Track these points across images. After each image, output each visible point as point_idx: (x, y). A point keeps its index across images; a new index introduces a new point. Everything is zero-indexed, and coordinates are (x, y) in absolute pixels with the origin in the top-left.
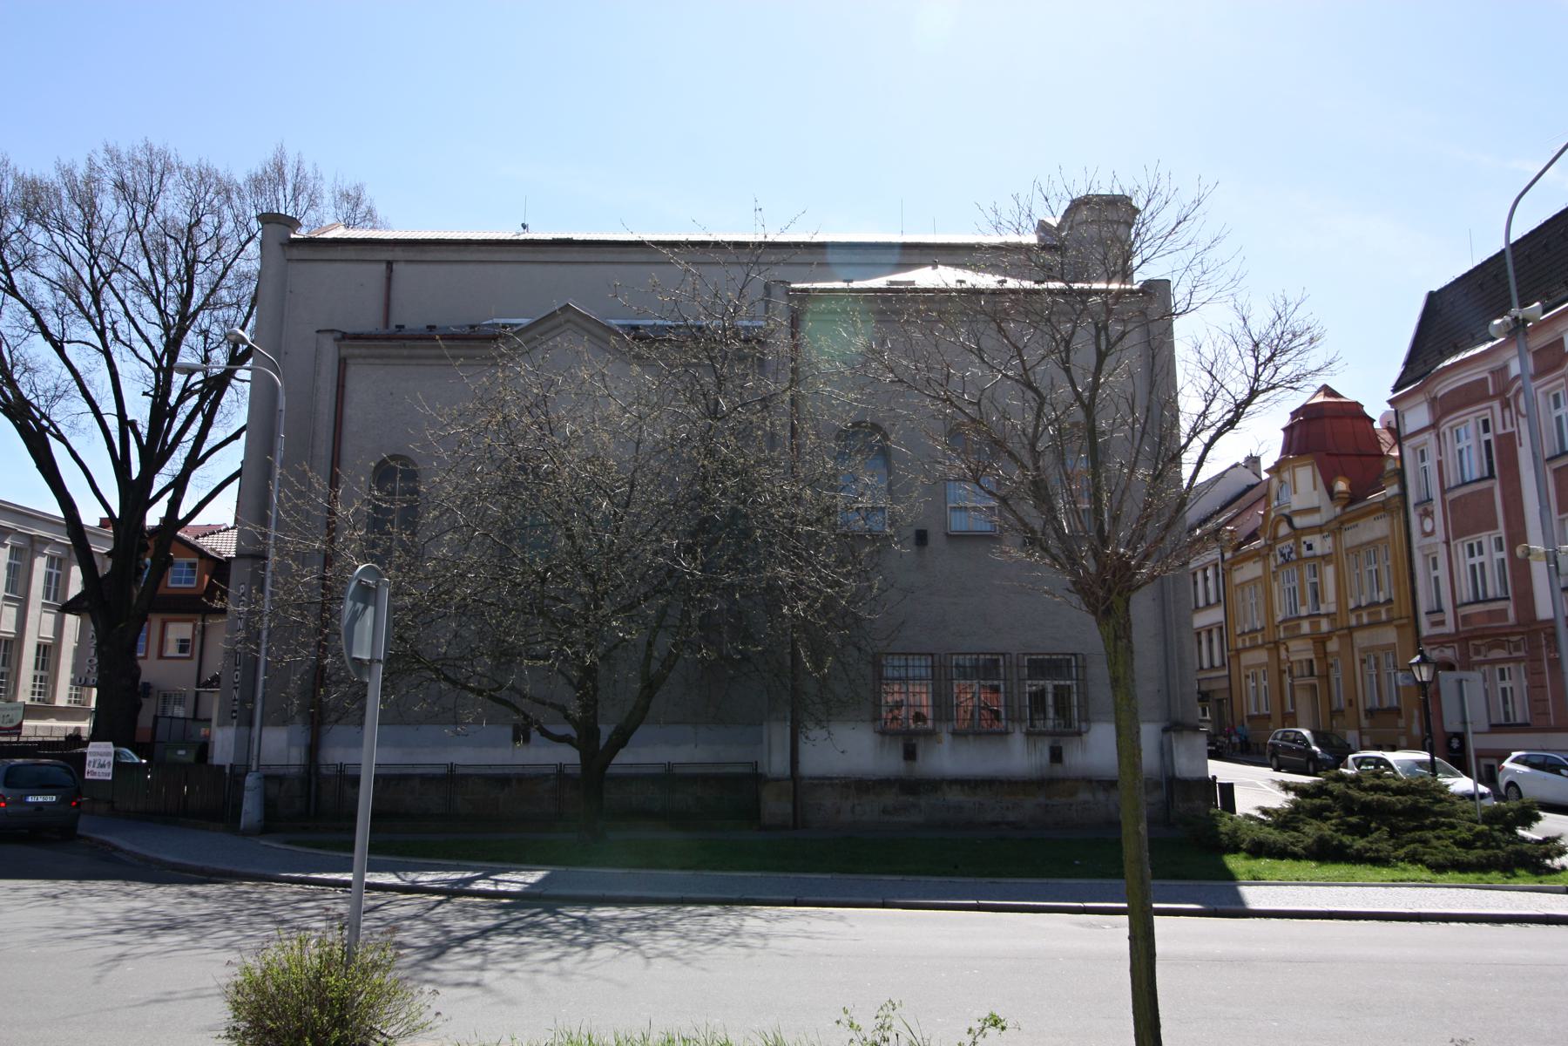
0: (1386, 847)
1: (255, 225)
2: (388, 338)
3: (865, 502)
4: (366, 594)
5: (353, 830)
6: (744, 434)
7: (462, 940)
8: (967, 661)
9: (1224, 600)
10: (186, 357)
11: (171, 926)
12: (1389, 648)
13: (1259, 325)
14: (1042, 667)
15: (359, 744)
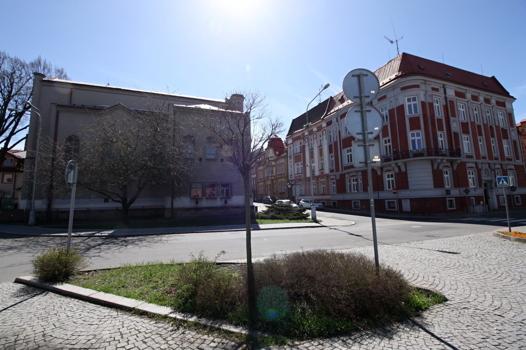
0: (283, 216)
1: (32, 75)
2: (71, 107)
3: (190, 151)
4: (71, 167)
5: (68, 223)
6: (163, 136)
7: (94, 247)
8: (208, 184)
9: (256, 173)
10: (10, 106)
11: (11, 248)
12: (283, 182)
13: (274, 121)
14: (225, 185)
15: (70, 203)
